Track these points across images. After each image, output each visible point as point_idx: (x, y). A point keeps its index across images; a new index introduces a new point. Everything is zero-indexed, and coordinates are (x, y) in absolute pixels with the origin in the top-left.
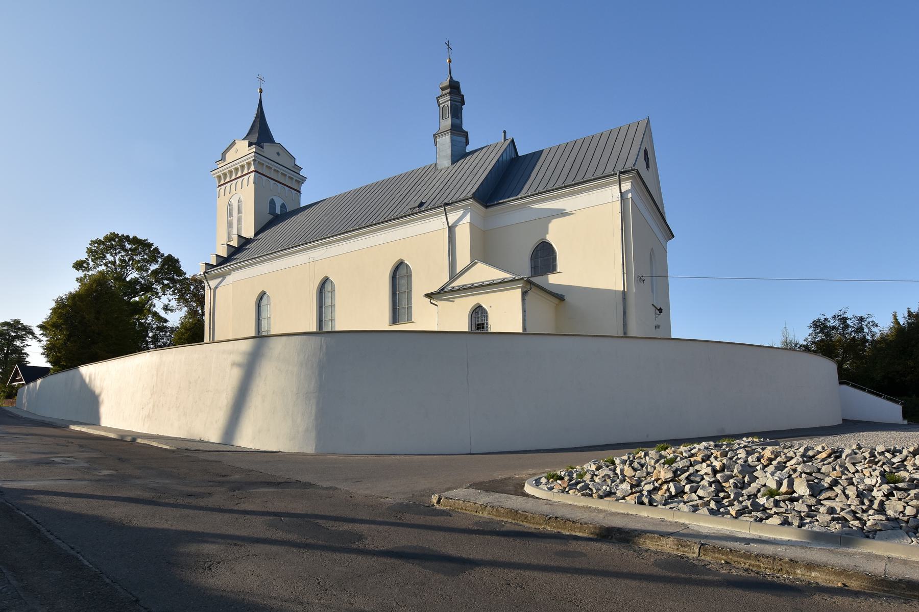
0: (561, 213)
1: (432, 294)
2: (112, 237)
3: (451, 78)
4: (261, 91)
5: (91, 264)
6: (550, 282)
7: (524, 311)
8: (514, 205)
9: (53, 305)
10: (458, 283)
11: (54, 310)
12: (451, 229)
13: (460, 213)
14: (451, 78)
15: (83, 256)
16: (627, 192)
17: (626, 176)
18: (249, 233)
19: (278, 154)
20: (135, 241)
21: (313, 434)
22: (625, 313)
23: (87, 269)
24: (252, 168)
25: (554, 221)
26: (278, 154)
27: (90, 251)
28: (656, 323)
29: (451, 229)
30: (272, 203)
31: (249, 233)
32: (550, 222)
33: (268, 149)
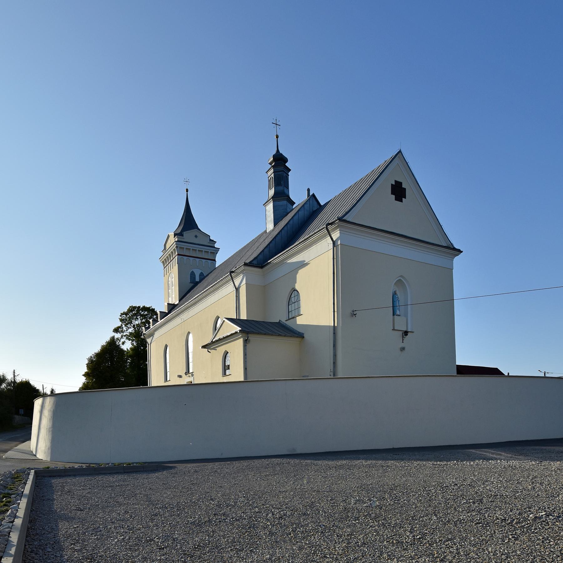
0: (303, 265)
1: (207, 345)
2: (132, 309)
3: (278, 151)
4: (187, 190)
5: (125, 329)
6: (298, 323)
7: (245, 355)
8: (276, 263)
9: (87, 362)
10: (220, 336)
11: (88, 365)
12: (237, 289)
13: (241, 276)
14: (278, 151)
15: (119, 324)
16: (337, 239)
17: (333, 226)
18: (175, 300)
19: (196, 236)
20: (145, 309)
21: (50, 451)
22: (334, 346)
23: (122, 332)
24: (176, 254)
25: (300, 271)
26: (196, 236)
27: (121, 320)
28: (402, 345)
29: (237, 289)
30: (193, 274)
31: (175, 300)
32: (297, 273)
33: (189, 236)
